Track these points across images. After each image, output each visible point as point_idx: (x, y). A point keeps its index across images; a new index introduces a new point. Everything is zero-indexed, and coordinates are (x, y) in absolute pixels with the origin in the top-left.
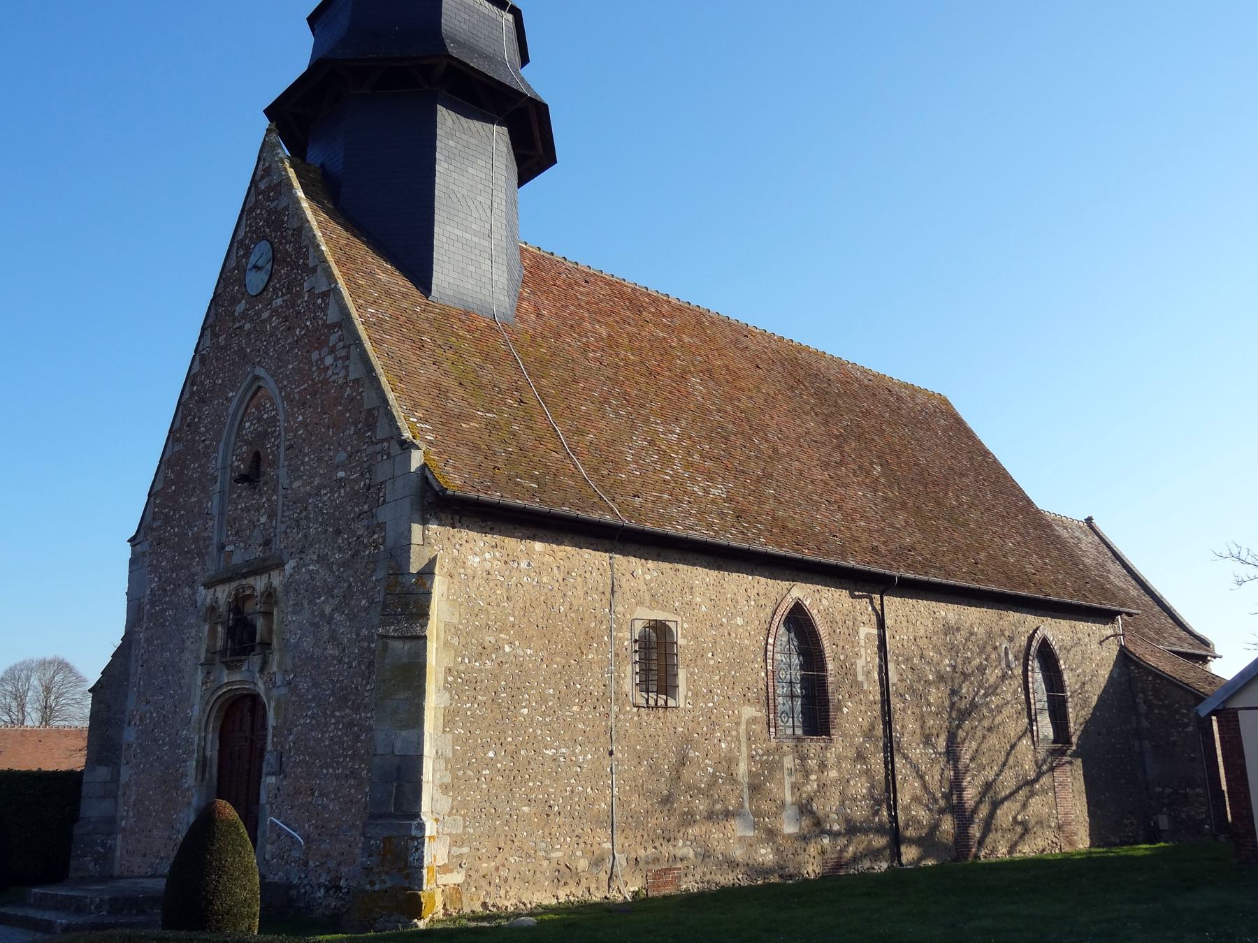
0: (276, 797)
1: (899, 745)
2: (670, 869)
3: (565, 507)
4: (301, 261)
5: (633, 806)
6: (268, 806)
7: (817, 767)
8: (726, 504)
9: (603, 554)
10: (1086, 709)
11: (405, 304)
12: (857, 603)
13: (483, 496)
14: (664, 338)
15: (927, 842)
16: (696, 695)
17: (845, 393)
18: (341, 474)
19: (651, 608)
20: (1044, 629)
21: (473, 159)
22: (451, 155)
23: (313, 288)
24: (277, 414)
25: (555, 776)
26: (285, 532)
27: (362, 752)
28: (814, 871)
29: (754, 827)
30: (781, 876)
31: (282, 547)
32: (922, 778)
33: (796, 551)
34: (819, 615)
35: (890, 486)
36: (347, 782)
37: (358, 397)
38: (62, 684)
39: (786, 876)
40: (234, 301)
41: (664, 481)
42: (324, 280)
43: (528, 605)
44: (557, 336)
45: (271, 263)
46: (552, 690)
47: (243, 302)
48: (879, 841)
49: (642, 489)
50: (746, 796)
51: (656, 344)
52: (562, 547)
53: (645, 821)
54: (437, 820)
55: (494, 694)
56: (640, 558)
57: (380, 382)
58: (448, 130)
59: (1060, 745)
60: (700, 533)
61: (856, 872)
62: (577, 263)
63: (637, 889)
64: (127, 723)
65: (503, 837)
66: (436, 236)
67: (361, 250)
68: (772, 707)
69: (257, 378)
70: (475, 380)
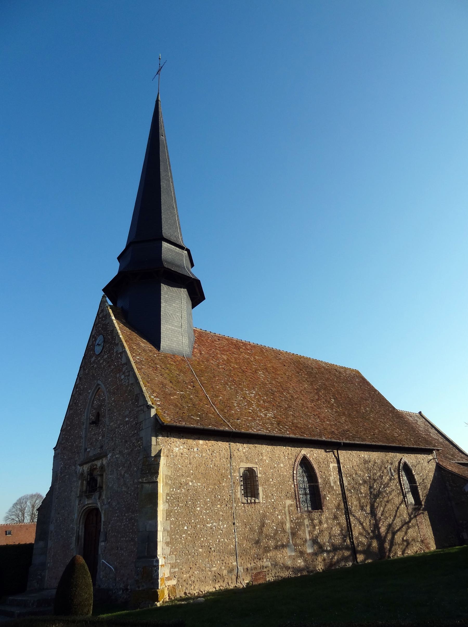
0: (104, 551)
1: (351, 511)
2: (261, 572)
3: (210, 426)
4: (113, 341)
5: (244, 545)
6: (101, 555)
7: (318, 523)
8: (274, 420)
9: (226, 443)
10: (426, 490)
11: (151, 354)
12: (328, 454)
13: (178, 424)
14: (248, 358)
15: (367, 552)
16: (267, 497)
17: (319, 372)
18: (127, 419)
19: (246, 463)
20: (404, 459)
21: (174, 301)
22: (166, 300)
23: (117, 351)
24: (105, 397)
25: (212, 535)
26: (108, 442)
27: (136, 530)
28: (321, 568)
29: (295, 551)
30: (308, 572)
31: (107, 448)
32: (362, 524)
33: (301, 436)
34: (313, 460)
35: (338, 407)
36: (130, 543)
37: (133, 390)
38: (39, 504)
39: (310, 571)
40: (91, 357)
41: (249, 412)
42: (121, 348)
43: (198, 465)
44: (208, 361)
45: (103, 343)
46: (209, 499)
47: (94, 357)
48: (347, 553)
49: (241, 416)
50: (290, 538)
51: (245, 360)
52: (210, 442)
53: (249, 552)
54: (164, 558)
55: (186, 503)
56: (241, 443)
57: (140, 384)
58: (165, 292)
59: (417, 506)
60: (264, 432)
61: (339, 568)
62: (215, 333)
63: (248, 582)
64: (51, 522)
65: (192, 563)
66: (162, 329)
67: (135, 336)
68: (298, 499)
69: (98, 385)
70: (176, 380)
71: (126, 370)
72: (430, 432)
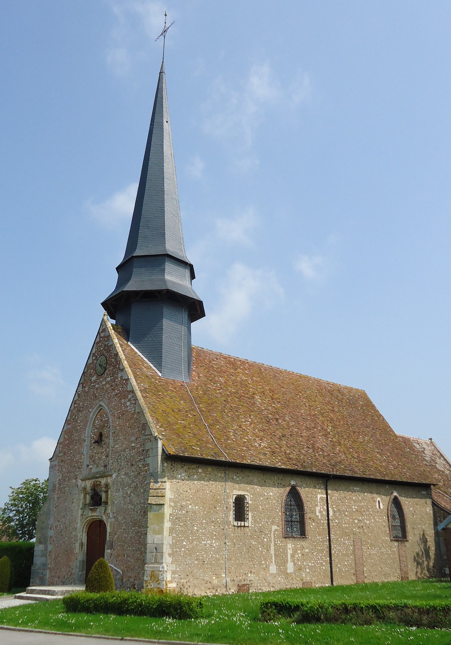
14: (246, 380)
18: (133, 445)
44: (206, 385)
60: (257, 462)
69: (100, 405)
71: (132, 397)
72: (437, 463)
